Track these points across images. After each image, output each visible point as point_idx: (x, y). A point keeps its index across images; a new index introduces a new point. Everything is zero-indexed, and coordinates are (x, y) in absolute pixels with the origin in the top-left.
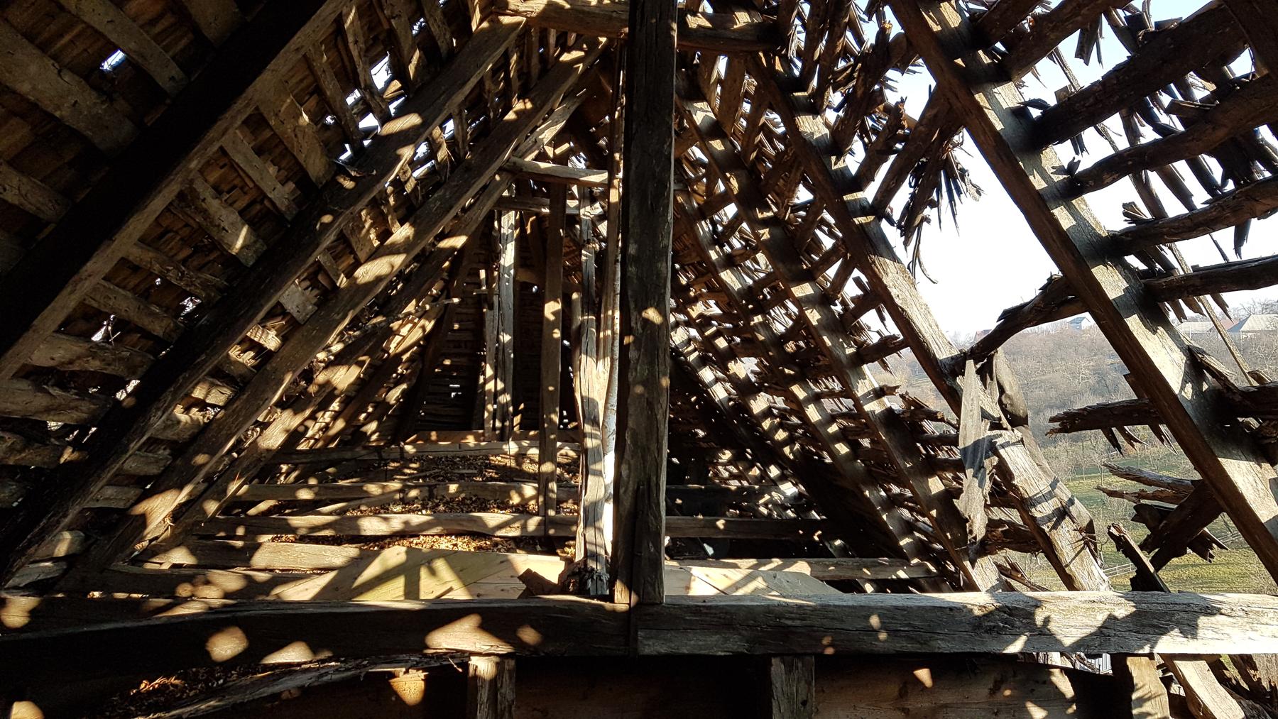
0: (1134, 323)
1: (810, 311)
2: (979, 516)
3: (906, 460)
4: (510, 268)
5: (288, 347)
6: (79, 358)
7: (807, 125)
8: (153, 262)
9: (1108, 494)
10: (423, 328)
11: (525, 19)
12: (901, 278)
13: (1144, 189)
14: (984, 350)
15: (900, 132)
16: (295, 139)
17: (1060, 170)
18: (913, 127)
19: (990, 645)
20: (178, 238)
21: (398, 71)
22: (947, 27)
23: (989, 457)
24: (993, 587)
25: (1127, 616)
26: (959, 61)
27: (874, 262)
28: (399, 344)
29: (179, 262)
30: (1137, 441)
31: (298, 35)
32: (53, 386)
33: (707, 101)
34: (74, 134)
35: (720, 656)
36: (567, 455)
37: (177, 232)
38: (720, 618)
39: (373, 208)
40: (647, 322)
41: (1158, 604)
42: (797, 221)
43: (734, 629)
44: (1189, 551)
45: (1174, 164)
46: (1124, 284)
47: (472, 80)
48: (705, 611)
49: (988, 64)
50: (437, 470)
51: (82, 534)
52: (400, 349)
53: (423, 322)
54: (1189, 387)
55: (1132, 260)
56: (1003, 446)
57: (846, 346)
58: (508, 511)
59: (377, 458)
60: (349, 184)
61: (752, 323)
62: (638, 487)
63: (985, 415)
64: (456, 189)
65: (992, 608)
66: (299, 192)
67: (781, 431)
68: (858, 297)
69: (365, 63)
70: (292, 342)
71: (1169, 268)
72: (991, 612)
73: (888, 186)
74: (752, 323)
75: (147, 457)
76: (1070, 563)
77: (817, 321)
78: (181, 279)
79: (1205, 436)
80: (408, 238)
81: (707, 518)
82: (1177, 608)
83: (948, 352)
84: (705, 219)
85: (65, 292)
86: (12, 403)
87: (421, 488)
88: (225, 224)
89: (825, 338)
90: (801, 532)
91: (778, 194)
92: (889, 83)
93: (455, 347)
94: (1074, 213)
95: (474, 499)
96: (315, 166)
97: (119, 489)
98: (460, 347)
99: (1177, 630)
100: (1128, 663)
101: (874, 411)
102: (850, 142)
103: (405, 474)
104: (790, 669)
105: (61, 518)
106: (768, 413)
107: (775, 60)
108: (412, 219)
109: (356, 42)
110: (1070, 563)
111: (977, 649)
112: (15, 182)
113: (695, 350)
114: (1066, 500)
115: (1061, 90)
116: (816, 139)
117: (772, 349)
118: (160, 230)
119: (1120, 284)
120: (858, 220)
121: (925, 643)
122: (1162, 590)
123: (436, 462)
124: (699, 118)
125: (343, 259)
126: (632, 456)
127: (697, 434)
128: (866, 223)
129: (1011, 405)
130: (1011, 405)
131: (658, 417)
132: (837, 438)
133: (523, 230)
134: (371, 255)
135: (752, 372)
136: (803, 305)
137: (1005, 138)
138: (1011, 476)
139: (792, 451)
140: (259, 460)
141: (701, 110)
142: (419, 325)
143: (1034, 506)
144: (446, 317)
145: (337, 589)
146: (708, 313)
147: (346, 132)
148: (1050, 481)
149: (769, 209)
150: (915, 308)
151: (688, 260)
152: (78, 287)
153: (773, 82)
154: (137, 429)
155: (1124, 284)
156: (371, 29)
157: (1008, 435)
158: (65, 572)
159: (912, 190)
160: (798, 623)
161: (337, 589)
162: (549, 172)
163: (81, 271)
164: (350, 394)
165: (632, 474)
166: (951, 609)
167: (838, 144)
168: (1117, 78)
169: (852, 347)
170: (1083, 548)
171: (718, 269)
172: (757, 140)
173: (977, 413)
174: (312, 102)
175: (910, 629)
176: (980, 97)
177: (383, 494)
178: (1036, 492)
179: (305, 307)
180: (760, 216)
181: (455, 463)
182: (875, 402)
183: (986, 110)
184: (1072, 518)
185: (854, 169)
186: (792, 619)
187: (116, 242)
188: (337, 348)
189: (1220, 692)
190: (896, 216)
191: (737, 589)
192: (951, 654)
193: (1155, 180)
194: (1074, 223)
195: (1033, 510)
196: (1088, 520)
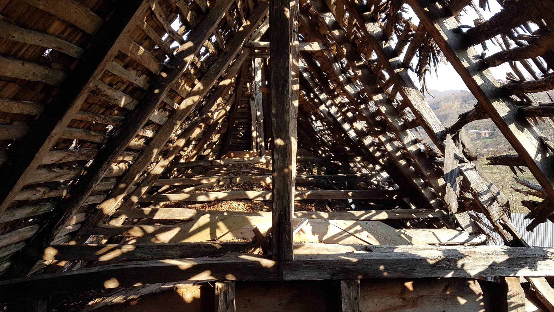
0: (513, 127)
1: (381, 107)
2: (454, 203)
3: (427, 171)
4: (259, 82)
5: (157, 136)
6: (64, 158)
8: (88, 118)
9: (515, 190)
13: (514, 68)
14: (455, 130)
15: (410, 33)
17: (477, 57)
18: (416, 29)
19: (439, 274)
20: (98, 106)
21: (184, 21)
23: (459, 176)
26: (426, 9)
27: (404, 89)
29: (101, 114)
30: (524, 171)
31: (127, 26)
32: (56, 168)
33: (331, 12)
34: (37, 83)
35: (318, 281)
37: (97, 104)
38: (318, 265)
39: (185, 76)
41: (520, 254)
42: (374, 66)
43: (323, 269)
44: (548, 220)
45: (527, 59)
46: (508, 110)
47: (217, 21)
48: (311, 262)
49: (441, 8)
50: (234, 170)
51: (85, 214)
54: (539, 156)
55: (514, 97)
56: (465, 170)
57: (398, 122)
58: (261, 189)
59: (211, 165)
61: (360, 109)
63: (456, 157)
64: (221, 63)
65: (440, 259)
66: (149, 78)
67: (378, 152)
68: (402, 101)
69: (166, 23)
71: (529, 102)
72: (440, 261)
73: (408, 55)
74: (360, 109)
75: (105, 184)
77: (385, 111)
79: (547, 178)
82: (529, 256)
83: (440, 129)
84: (337, 62)
85: (47, 142)
86: (40, 178)
88: (117, 97)
89: (389, 118)
91: (365, 54)
92: (405, 9)
93: (241, 115)
94: (483, 77)
95: (248, 183)
96: (153, 67)
97: (96, 196)
98: (243, 115)
100: (506, 279)
101: (412, 150)
102: (391, 34)
103: (221, 173)
104: (349, 285)
105: (69, 215)
106: (372, 144)
109: (161, 16)
112: (16, 105)
113: (340, 116)
114: (496, 193)
115: (476, 20)
116: (376, 34)
118: (88, 105)
119: (506, 109)
120: (396, 71)
121: (409, 274)
122: (524, 246)
123: (234, 166)
124: (327, 20)
125: (176, 98)
126: (278, 200)
127: (346, 149)
128: (400, 72)
129: (469, 153)
130: (469, 153)
131: (288, 183)
132: (400, 158)
133: (265, 63)
134: (188, 95)
135: (364, 127)
136: (378, 104)
137: (449, 44)
138: (469, 183)
139: (383, 161)
141: (328, 16)
143: (480, 196)
144: (236, 102)
146: (343, 102)
147: (164, 50)
148: (488, 184)
149: (361, 60)
150: (424, 110)
151: (332, 79)
152: (51, 139)
153: (354, 9)
154: (94, 179)
155: (508, 110)
156: (167, 8)
157: (468, 165)
158: (81, 228)
159: (418, 58)
160: (352, 267)
162: (266, 46)
163: (51, 134)
164: (200, 137)
165: (278, 208)
166: (421, 260)
167: (385, 36)
168: (496, 20)
169: (402, 122)
170: (503, 214)
172: (353, 30)
173: (452, 157)
174: (147, 43)
175: (402, 268)
176: (437, 26)
179: (162, 119)
180: (357, 64)
181: (242, 167)
182: (413, 146)
183: (440, 32)
184: (497, 201)
185: (394, 47)
186: (349, 265)
187: (64, 120)
188: (179, 132)
189: (551, 291)
190: (414, 68)
192: (421, 278)
193: (518, 64)
194: (484, 82)
195: (479, 198)
196: (507, 201)
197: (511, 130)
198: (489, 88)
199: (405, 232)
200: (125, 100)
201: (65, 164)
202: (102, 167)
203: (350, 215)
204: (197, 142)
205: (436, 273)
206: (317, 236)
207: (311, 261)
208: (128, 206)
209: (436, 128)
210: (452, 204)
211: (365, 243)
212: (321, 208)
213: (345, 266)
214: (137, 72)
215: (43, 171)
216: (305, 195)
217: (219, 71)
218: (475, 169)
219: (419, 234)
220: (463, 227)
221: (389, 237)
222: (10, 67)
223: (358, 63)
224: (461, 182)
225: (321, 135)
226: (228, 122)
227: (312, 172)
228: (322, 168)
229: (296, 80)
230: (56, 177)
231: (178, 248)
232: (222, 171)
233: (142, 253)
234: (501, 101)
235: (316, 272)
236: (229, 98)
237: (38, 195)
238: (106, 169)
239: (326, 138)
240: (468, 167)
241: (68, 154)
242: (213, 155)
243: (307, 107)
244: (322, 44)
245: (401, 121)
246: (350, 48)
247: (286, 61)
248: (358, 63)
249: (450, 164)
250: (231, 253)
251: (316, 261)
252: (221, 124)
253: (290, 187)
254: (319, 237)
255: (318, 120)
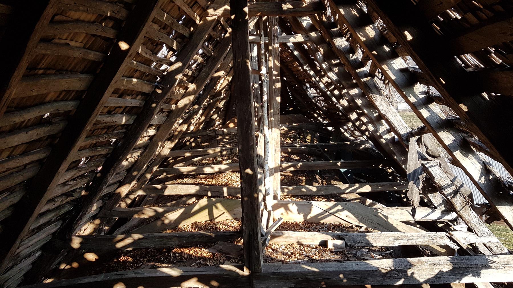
2: (416, 198)
4: (256, 57)
7: (338, 42)
10: (228, 80)
11: (217, 17)
12: (383, 102)
16: (134, 87)
22: (369, 38)
24: (440, 204)
25: (449, 271)
26: (374, 52)
27: (371, 96)
28: (220, 86)
31: (113, 79)
36: (284, 129)
40: (247, 174)
41: (464, 264)
43: (288, 280)
47: (200, 44)
48: (278, 274)
50: (235, 140)
52: (221, 88)
53: (227, 78)
54: (483, 179)
56: (430, 167)
57: (374, 113)
60: (159, 91)
61: (342, 93)
62: (250, 233)
65: (389, 269)
70: (160, 130)
72: (390, 271)
74: (342, 93)
76: (460, 211)
77: (361, 104)
78: (106, 139)
80: (194, 88)
81: (334, 161)
82: (472, 266)
83: (405, 131)
87: (228, 150)
90: (373, 165)
99: (471, 275)
101: (387, 138)
102: (357, 49)
103: (224, 142)
107: (322, 17)
108: (195, 81)
110: (460, 211)
111: (384, 284)
117: (352, 103)
119: (451, 138)
127: (339, 114)
128: (367, 81)
130: (432, 153)
137: (396, 82)
138: (434, 178)
140: (163, 158)
141: (306, 20)
142: (226, 79)
143: (444, 190)
145: (186, 214)
150: (390, 114)
157: (432, 162)
160: (313, 277)
161: (186, 214)
162: (253, 41)
163: (58, 171)
169: (377, 113)
170: (466, 205)
171: (326, 72)
177: (214, 153)
178: (445, 184)
179: (161, 120)
180: (334, 62)
182: (388, 134)
183: (387, 72)
186: (311, 276)
191: (331, 209)
194: (430, 115)
196: (470, 192)
197: (456, 156)
198: (435, 120)
199: (381, 211)
200: (126, 118)
201: (78, 177)
202: (110, 173)
203: (335, 189)
204: (204, 110)
205: (386, 282)
206: (302, 215)
207: (277, 273)
208: (140, 185)
209: (401, 130)
210: (414, 199)
211: (345, 221)
212: (311, 179)
213: (307, 276)
214: (132, 96)
215: (59, 187)
216: (298, 165)
217: (209, 75)
218: (440, 166)
219: (394, 213)
220: (436, 205)
221: (366, 216)
222: (16, 139)
223: (334, 61)
224: (424, 179)
225: (315, 100)
226: (231, 91)
227: (306, 139)
228: (316, 134)
229: (278, 79)
230: (71, 187)
231: (176, 238)
232: (225, 140)
233: (147, 243)
234: (446, 131)
235: (282, 281)
236: (230, 71)
237: (57, 204)
238: (113, 173)
239: (320, 103)
240: (432, 164)
241: (78, 171)
242: (219, 119)
243: (301, 76)
244: (305, 35)
245: (376, 113)
246: (326, 48)
247: (249, 106)
248: (334, 61)
249: (413, 164)
250: (221, 243)
251: (282, 272)
252: (224, 93)
253: (257, 211)
254: (304, 216)
255: (312, 88)
